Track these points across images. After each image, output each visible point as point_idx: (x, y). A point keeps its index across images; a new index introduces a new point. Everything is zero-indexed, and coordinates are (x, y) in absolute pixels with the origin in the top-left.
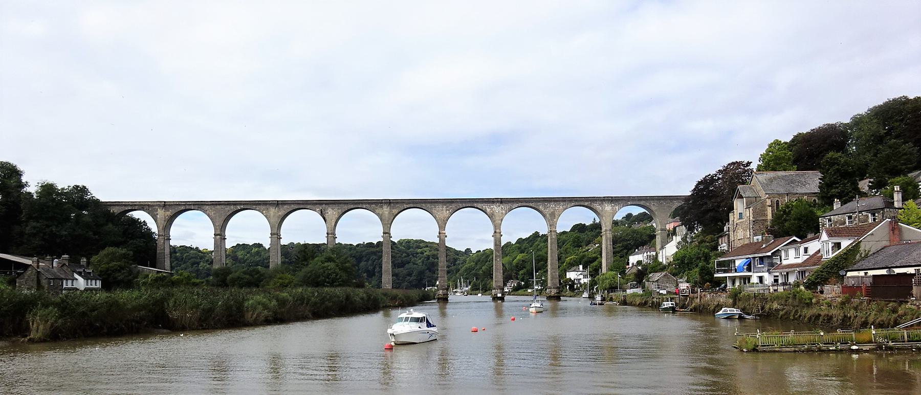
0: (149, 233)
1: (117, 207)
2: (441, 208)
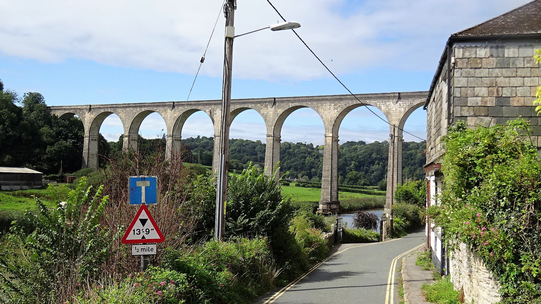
1: (60, 111)
2: (329, 107)
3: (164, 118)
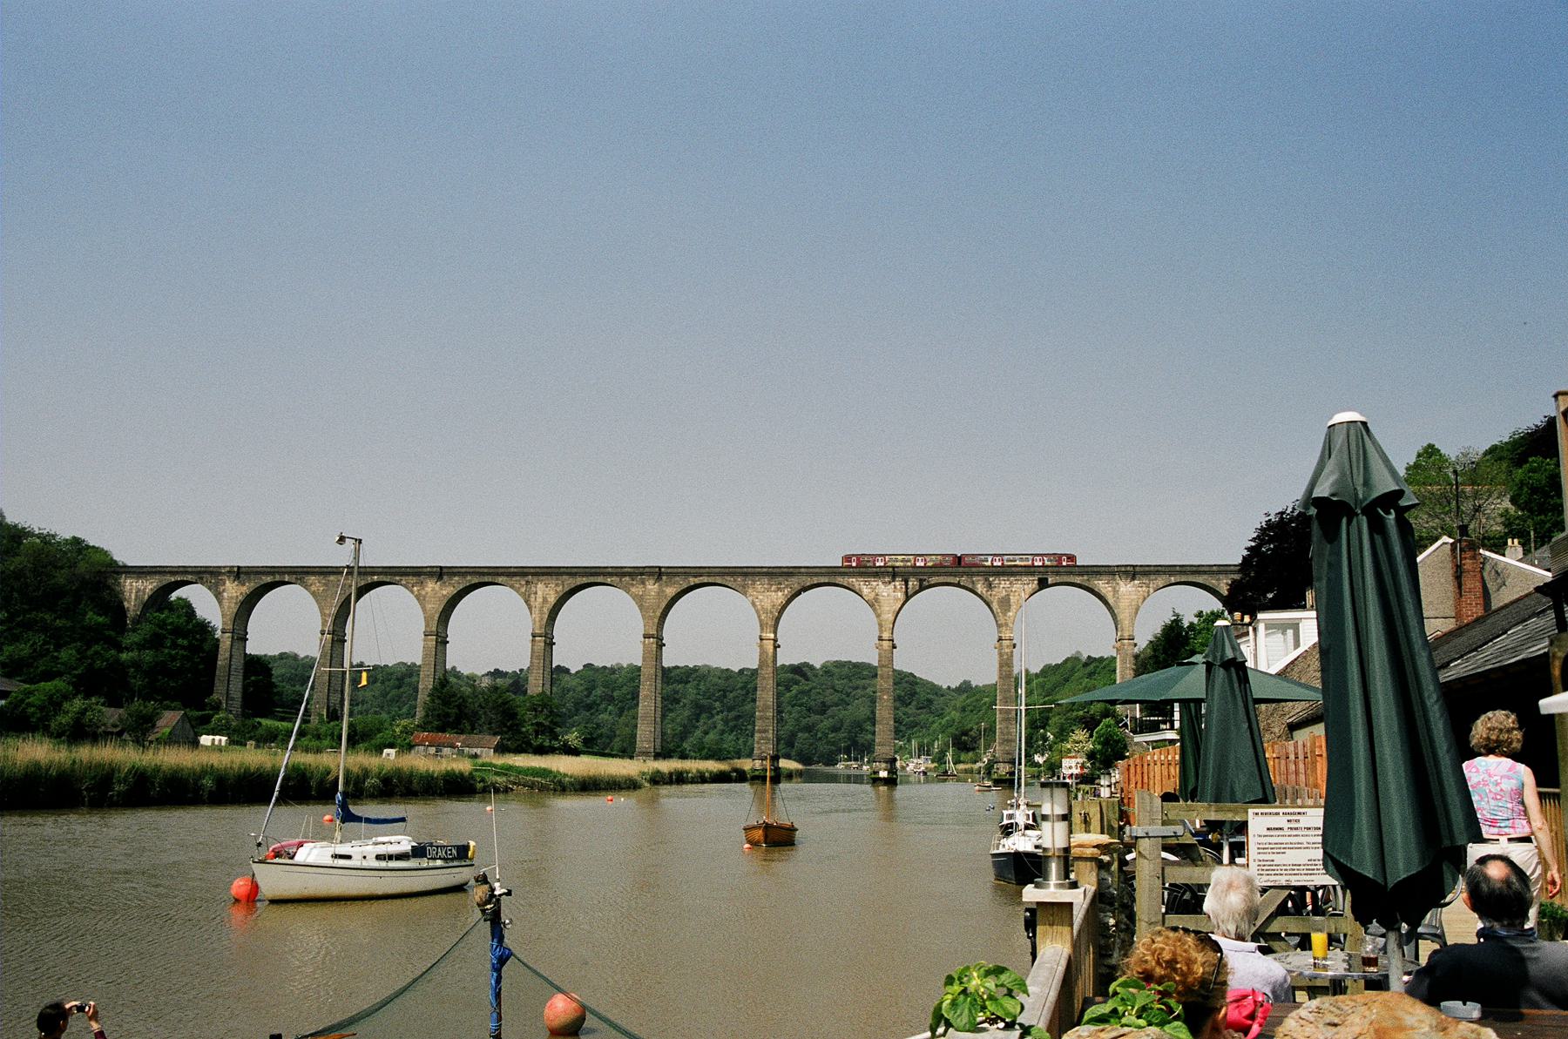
0: (204, 628)
3: (418, 597)
